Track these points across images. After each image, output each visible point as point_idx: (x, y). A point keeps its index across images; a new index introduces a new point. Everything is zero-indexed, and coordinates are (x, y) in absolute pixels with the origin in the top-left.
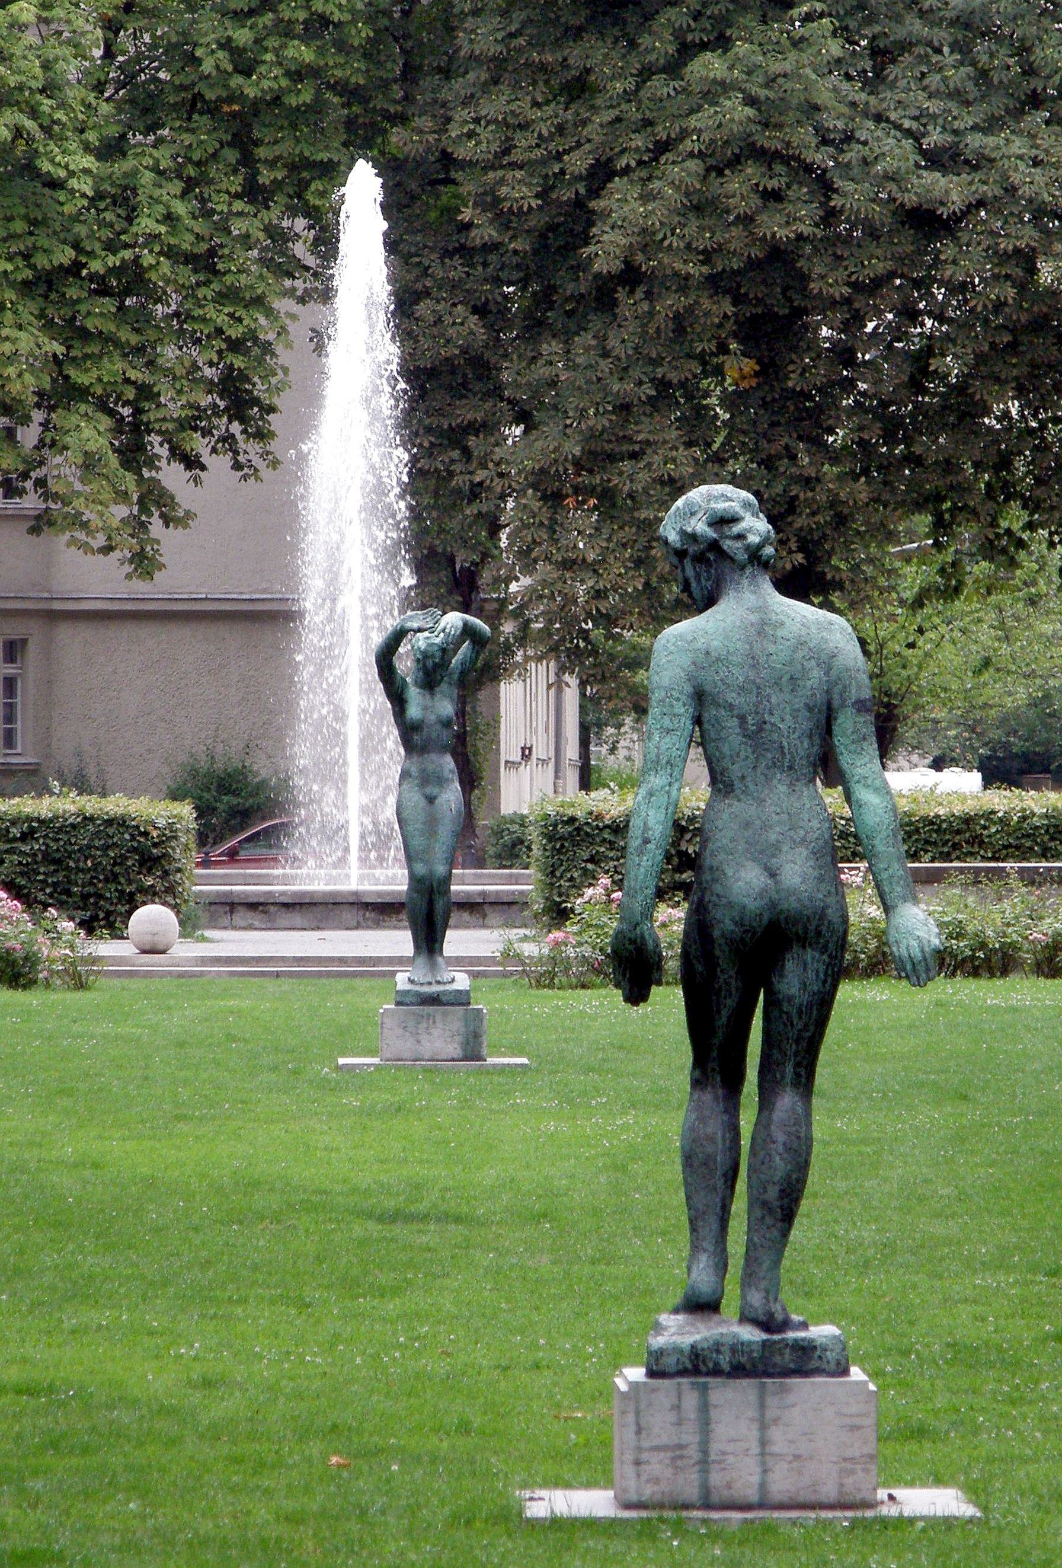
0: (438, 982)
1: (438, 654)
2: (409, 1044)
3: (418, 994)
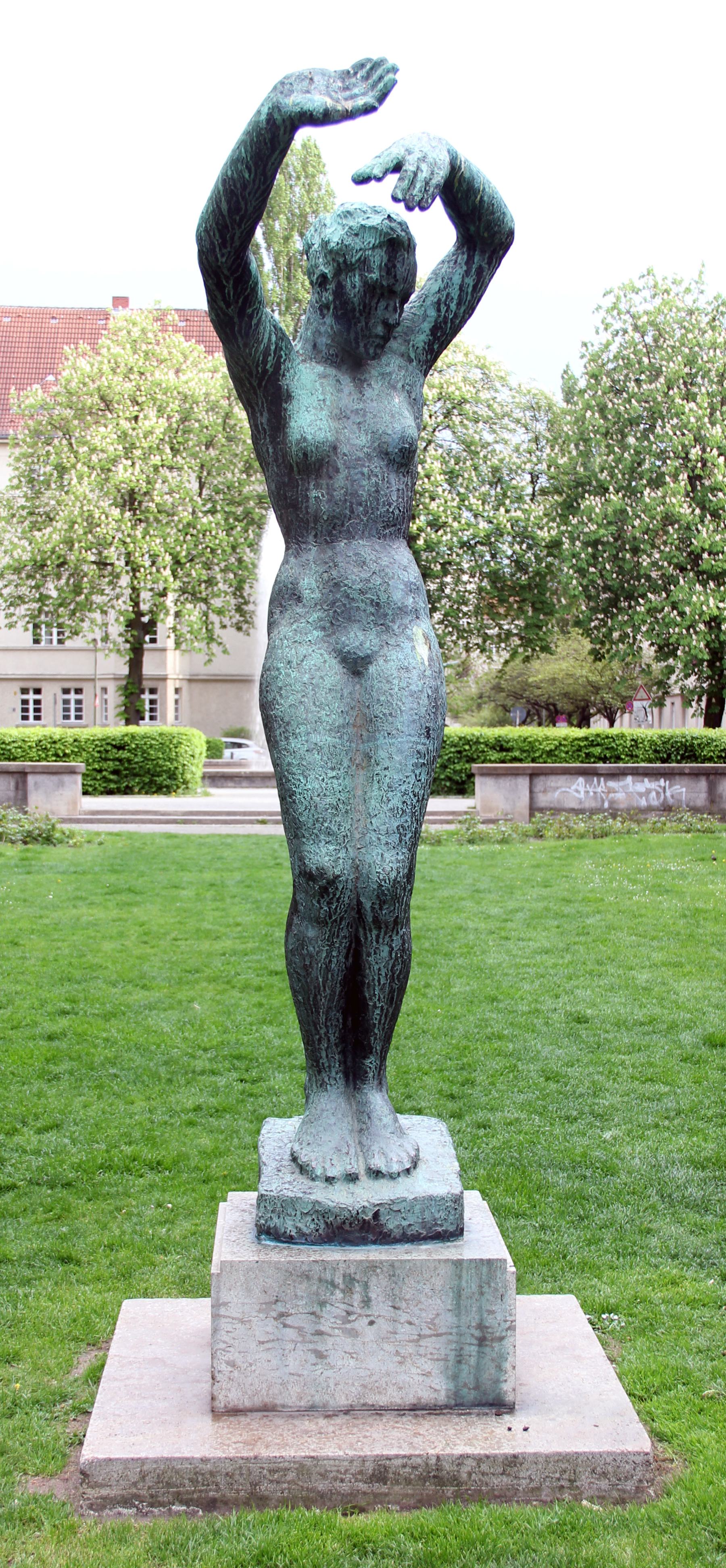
0: (376, 1174)
1: (378, 258)
2: (293, 1363)
3: (320, 1212)
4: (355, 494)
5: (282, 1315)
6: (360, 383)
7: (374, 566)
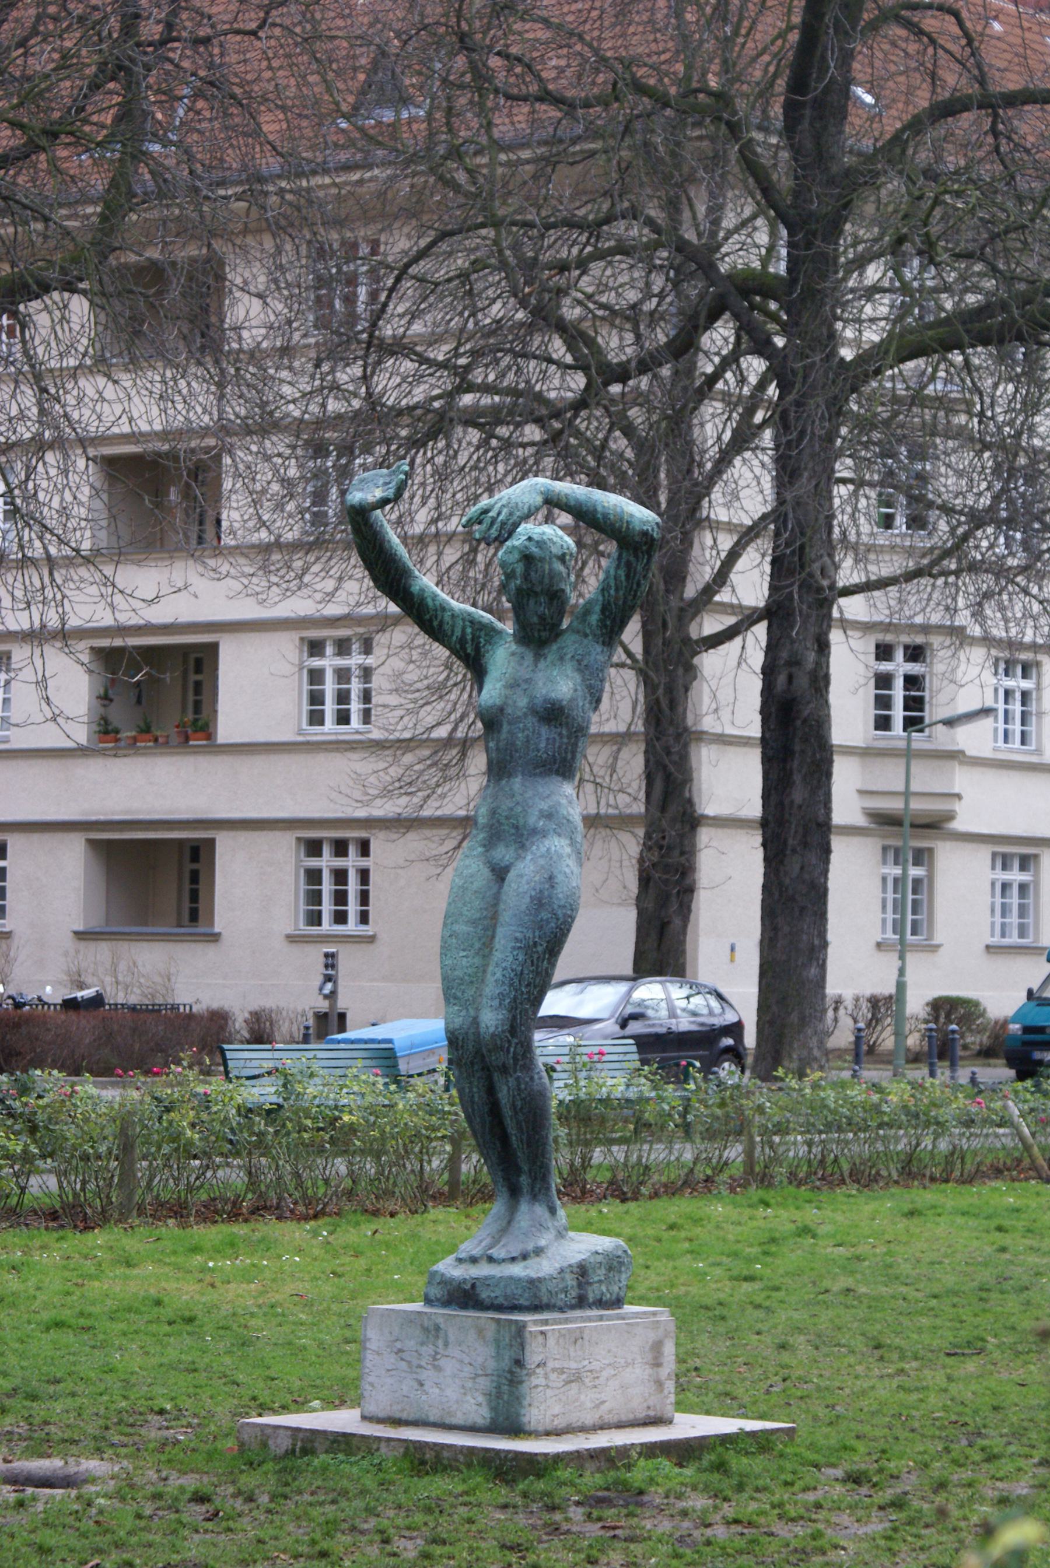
4: (513, 744)
5: (400, 1351)
6: (538, 656)
7: (519, 798)
